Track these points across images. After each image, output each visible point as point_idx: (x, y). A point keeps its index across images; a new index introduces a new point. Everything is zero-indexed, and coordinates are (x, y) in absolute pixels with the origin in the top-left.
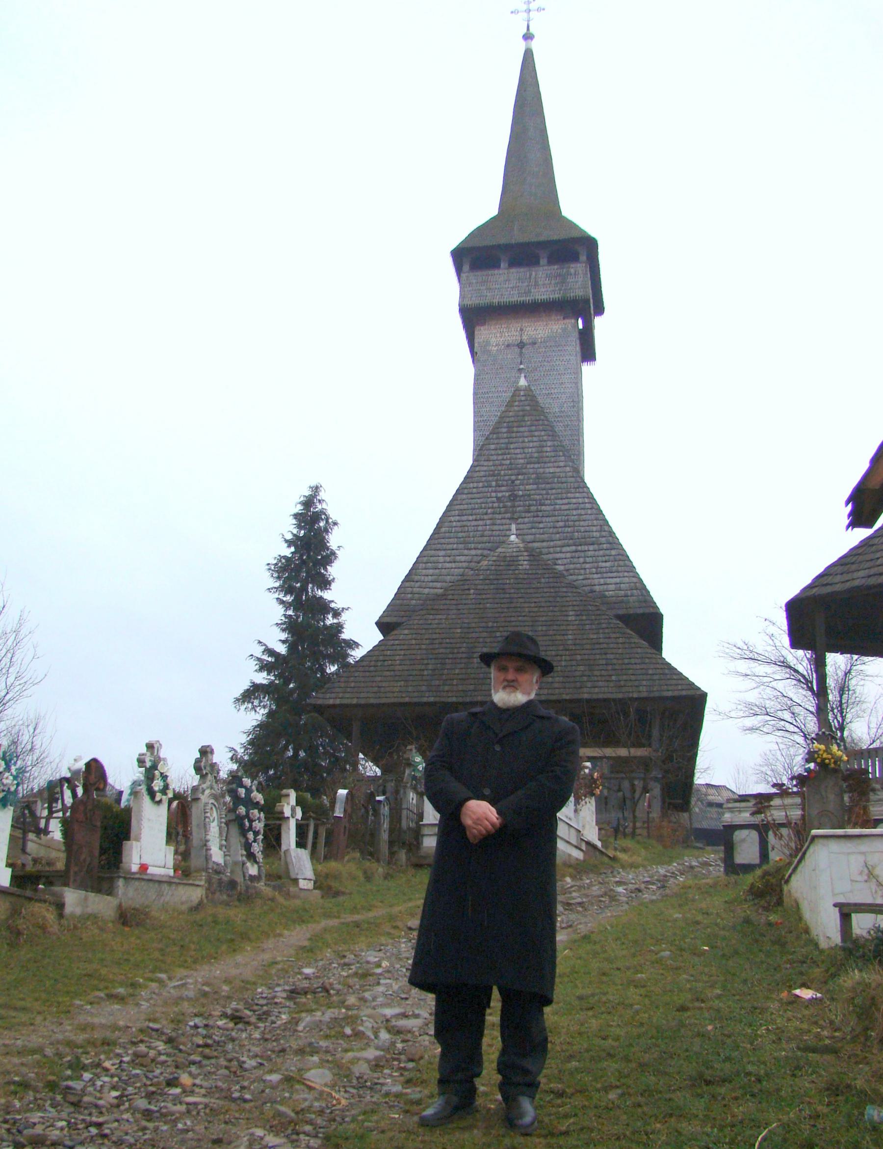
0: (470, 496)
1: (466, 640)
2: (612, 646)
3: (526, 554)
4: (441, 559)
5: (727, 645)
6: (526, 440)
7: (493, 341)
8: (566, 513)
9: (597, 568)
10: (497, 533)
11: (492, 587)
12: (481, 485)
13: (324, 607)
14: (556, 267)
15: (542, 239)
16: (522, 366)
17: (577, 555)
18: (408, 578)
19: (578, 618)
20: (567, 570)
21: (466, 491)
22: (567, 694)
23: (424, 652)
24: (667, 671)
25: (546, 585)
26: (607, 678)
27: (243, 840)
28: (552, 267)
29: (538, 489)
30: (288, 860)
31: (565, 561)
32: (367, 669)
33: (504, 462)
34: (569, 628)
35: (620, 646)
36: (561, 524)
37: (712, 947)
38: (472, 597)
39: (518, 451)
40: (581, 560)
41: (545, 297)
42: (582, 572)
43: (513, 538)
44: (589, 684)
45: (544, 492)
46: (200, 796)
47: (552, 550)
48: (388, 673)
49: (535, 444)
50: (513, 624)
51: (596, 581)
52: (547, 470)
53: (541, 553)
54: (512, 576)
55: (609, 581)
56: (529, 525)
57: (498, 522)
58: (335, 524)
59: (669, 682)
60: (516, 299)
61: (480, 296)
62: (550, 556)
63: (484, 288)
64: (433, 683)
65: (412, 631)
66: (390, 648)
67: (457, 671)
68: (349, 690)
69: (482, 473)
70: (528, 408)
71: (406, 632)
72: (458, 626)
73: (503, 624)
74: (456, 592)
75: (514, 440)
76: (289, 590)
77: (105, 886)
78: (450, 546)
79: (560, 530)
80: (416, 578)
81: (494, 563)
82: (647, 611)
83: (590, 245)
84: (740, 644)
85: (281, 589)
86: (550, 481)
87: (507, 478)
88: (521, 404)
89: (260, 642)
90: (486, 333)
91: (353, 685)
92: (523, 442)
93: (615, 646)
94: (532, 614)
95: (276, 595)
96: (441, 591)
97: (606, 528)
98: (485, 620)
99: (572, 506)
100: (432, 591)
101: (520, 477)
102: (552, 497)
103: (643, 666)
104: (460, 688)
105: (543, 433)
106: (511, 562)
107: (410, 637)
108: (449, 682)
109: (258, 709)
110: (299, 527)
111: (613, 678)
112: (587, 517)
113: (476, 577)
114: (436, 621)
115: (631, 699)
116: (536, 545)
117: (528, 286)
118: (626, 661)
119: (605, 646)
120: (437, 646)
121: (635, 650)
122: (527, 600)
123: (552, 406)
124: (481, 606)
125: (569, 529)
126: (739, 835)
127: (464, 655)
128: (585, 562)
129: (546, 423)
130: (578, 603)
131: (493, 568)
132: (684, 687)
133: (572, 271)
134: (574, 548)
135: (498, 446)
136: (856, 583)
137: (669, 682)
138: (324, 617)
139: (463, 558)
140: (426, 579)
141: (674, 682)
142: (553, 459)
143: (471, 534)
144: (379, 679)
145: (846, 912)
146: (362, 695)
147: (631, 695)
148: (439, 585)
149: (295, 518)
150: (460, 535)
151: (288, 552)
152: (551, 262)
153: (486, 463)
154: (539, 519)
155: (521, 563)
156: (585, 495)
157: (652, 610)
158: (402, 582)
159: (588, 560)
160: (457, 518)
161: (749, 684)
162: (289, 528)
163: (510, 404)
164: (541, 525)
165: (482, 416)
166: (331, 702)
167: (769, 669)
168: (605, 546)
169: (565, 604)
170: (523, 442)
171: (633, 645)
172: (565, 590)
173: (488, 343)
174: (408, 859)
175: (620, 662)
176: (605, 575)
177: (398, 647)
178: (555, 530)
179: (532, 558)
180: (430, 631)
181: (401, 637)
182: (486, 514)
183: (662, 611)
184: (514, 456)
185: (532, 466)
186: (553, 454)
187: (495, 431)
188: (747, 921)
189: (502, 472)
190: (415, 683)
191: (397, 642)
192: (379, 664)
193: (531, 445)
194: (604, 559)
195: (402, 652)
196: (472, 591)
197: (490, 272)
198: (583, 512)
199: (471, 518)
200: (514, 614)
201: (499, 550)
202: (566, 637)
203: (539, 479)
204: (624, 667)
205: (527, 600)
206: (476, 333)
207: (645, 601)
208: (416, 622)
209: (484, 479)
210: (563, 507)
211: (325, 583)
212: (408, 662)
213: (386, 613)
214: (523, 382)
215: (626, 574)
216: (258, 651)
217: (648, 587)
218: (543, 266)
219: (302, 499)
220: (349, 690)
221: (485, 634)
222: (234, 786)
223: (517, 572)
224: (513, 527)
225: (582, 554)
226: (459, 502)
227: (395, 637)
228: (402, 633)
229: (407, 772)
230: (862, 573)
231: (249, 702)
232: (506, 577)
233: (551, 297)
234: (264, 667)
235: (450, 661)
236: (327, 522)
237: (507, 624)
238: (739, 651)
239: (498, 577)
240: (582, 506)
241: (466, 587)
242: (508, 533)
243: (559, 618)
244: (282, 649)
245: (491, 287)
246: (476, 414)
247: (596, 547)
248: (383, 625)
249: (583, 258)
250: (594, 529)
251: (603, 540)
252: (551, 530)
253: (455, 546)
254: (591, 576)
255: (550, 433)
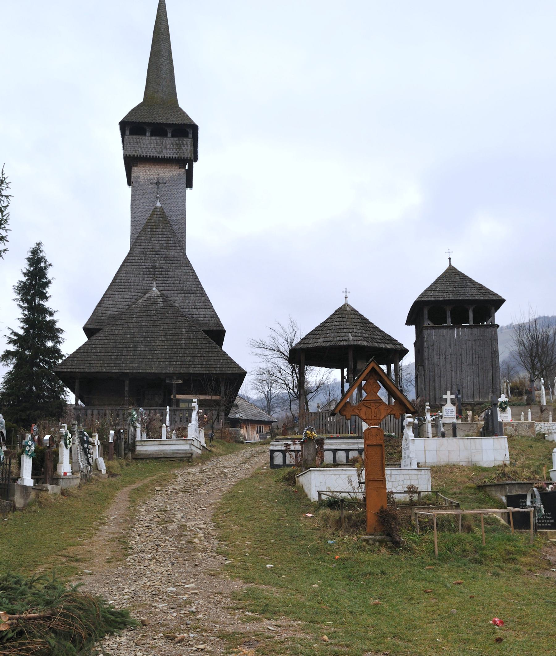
0: (131, 264)
1: (133, 341)
2: (203, 347)
3: (161, 298)
4: (117, 296)
5: (252, 341)
6: (160, 236)
7: (142, 176)
8: (180, 276)
9: (195, 306)
10: (145, 284)
11: (145, 314)
12: (137, 258)
13: (46, 311)
14: (176, 139)
15: (169, 122)
16: (158, 196)
17: (185, 298)
18: (100, 305)
19: (187, 332)
20: (180, 306)
21: (129, 261)
22: (183, 370)
23: (112, 346)
24: (229, 361)
25: (171, 315)
26: (202, 363)
27: (86, 457)
28: (174, 139)
29: (166, 263)
30: (97, 463)
31: (179, 301)
32: (83, 354)
33: (149, 247)
34: (183, 337)
35: (207, 347)
36: (177, 282)
37: (278, 500)
38: (135, 319)
39: (156, 242)
40: (187, 301)
41: (170, 156)
42: (188, 307)
43: (154, 289)
44: (193, 366)
45: (169, 265)
46: (75, 442)
47: (173, 295)
48: (94, 356)
49: (165, 239)
50: (156, 334)
51: (194, 313)
52: (171, 253)
53: (167, 297)
54: (155, 309)
55: (200, 313)
56: (162, 282)
57: (146, 279)
58: (50, 265)
59: (230, 366)
60: (154, 155)
61: (135, 151)
62: (172, 298)
63: (137, 146)
64: (117, 362)
65: (105, 335)
66: (94, 343)
67: (129, 357)
68: (74, 364)
69: (137, 252)
70: (161, 219)
71: (102, 335)
72: (128, 334)
73: (151, 334)
74: (127, 316)
75: (154, 236)
76: (27, 301)
77: (55, 482)
78: (121, 290)
79: (177, 285)
80: (104, 305)
81: (145, 302)
82: (218, 328)
83: (195, 128)
84: (259, 341)
85: (22, 300)
86: (172, 259)
87: (150, 256)
88: (158, 216)
89: (9, 328)
90: (139, 172)
91: (76, 362)
92: (159, 237)
93: (205, 347)
94: (164, 329)
95: (18, 303)
96: (117, 313)
97: (200, 286)
98: (142, 331)
99: (183, 273)
100: (112, 312)
101: (157, 256)
102: (173, 268)
103: (217, 358)
104: (131, 365)
105: (169, 233)
106: (153, 302)
107: (104, 338)
108: (125, 362)
109: (9, 365)
110: (31, 266)
111: (204, 363)
112: (191, 280)
113: (136, 309)
114: (117, 331)
115: (213, 373)
116: (165, 292)
117: (161, 148)
118: (210, 355)
119: (200, 347)
120: (118, 344)
121: (213, 350)
122: (162, 322)
123: (172, 216)
124: (140, 324)
125: (182, 285)
126: (276, 454)
127: (132, 349)
128: (189, 303)
129: (170, 228)
130: (187, 325)
131: (145, 304)
132: (237, 369)
133: (185, 142)
134: (183, 295)
135: (146, 238)
136: (318, 344)
137: (230, 366)
138: (45, 316)
139: (128, 297)
140: (109, 306)
141: (232, 366)
142: (173, 248)
143: (132, 284)
144: (89, 359)
145: (320, 494)
146: (81, 367)
147: (212, 372)
148: (116, 310)
149: (29, 261)
150: (126, 284)
151: (24, 279)
152: (173, 136)
153: (139, 247)
154: (166, 279)
155: (159, 302)
156: (189, 268)
157: (221, 329)
158: (96, 307)
159: (190, 301)
160: (125, 275)
161: (260, 359)
162: (25, 266)
163: (152, 215)
164: (168, 282)
165: (135, 218)
166: (65, 370)
167: (270, 352)
168: (199, 295)
169: (181, 325)
170: (159, 237)
171: (213, 348)
172: (180, 318)
173: (139, 178)
174: (132, 456)
175: (207, 355)
176: (198, 310)
177: (99, 343)
178: (174, 285)
179: (164, 300)
180: (114, 336)
181: (100, 338)
182: (140, 274)
183: (225, 329)
184: (154, 244)
185: (163, 250)
186: (174, 245)
187: (144, 230)
188: (285, 490)
189: (148, 253)
190: (108, 362)
191: (97, 341)
192: (89, 351)
193: (163, 239)
194: (198, 302)
195: (101, 346)
196: (135, 316)
197: (141, 137)
198: (188, 277)
199: (132, 276)
200: (156, 329)
201: (147, 295)
202: (181, 342)
203: (166, 258)
204: (209, 358)
205: (162, 322)
206: (132, 170)
207: (218, 324)
208: (107, 330)
209: (138, 255)
210: (179, 273)
211: (44, 297)
212: (104, 351)
213: (88, 323)
214: (158, 204)
215: (209, 310)
216: (8, 333)
217: (219, 317)
218: (169, 137)
219: (31, 249)
220: (74, 364)
221: (141, 339)
222: (82, 436)
223: (157, 307)
224: (154, 283)
225: (188, 298)
226: (125, 267)
227: (96, 338)
228: (99, 336)
229: (129, 418)
230: (321, 340)
231: (5, 361)
232: (151, 309)
233: (173, 156)
234: (11, 341)
235: (125, 352)
236: (45, 263)
237: (153, 334)
238: (257, 344)
239: (148, 309)
240: (188, 273)
241: (132, 313)
242: (151, 285)
243: (178, 332)
244: (21, 332)
245: (141, 146)
246: (132, 216)
247: (195, 295)
248: (88, 330)
249: (190, 136)
250: (194, 286)
251: (198, 292)
252: (172, 285)
253: (124, 290)
254: (192, 310)
255: (172, 234)
